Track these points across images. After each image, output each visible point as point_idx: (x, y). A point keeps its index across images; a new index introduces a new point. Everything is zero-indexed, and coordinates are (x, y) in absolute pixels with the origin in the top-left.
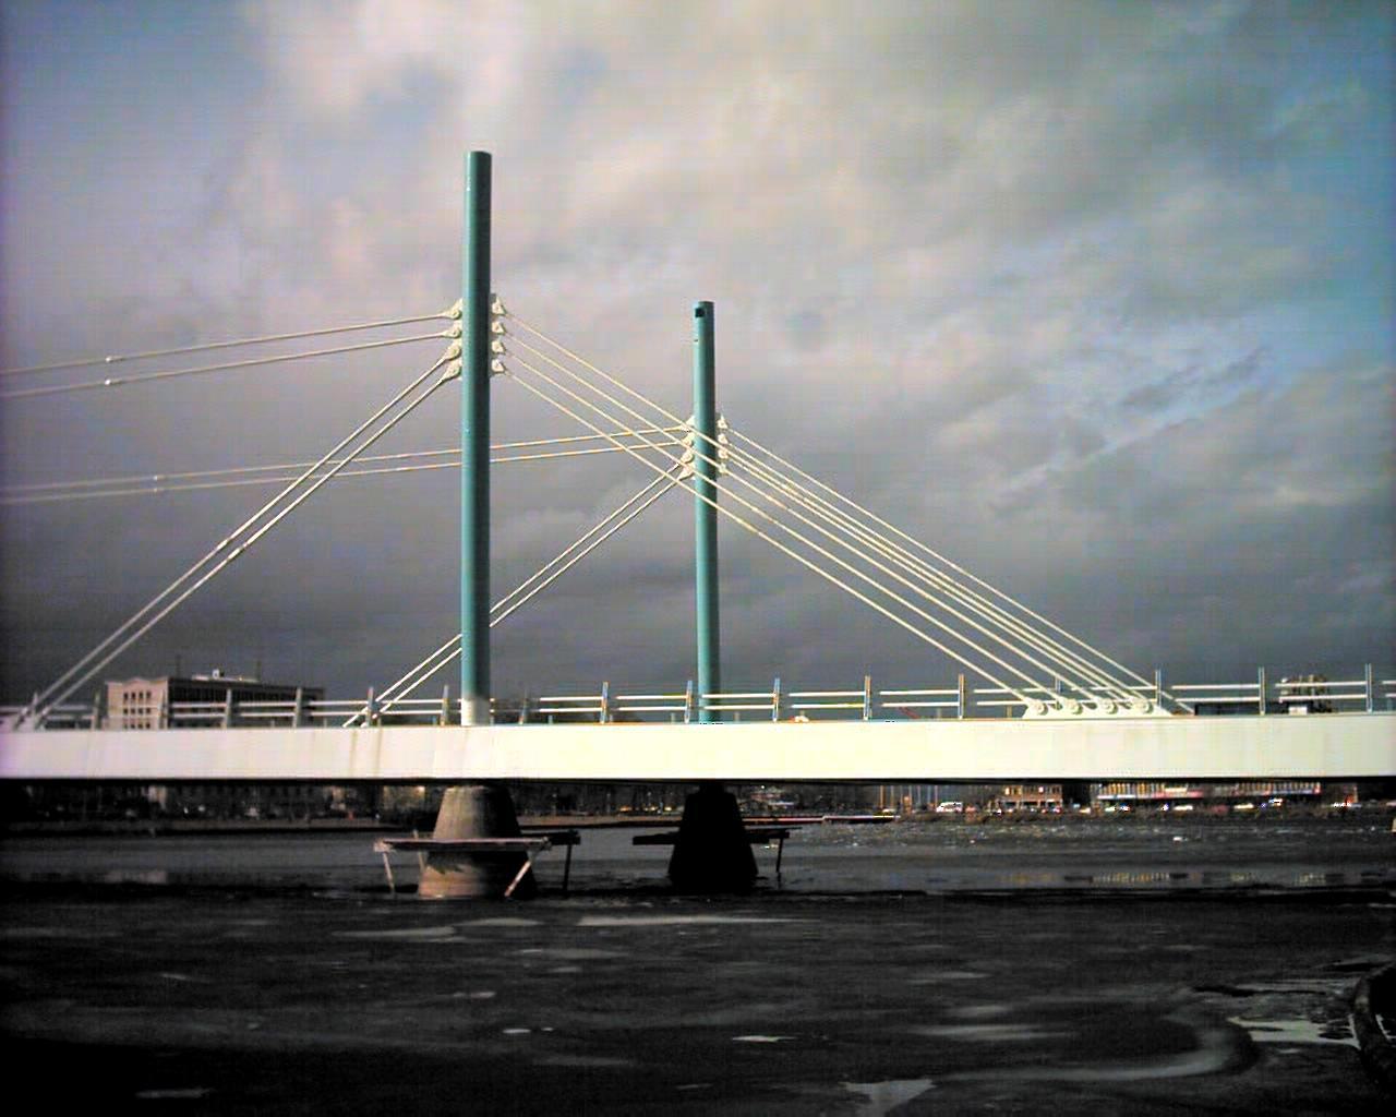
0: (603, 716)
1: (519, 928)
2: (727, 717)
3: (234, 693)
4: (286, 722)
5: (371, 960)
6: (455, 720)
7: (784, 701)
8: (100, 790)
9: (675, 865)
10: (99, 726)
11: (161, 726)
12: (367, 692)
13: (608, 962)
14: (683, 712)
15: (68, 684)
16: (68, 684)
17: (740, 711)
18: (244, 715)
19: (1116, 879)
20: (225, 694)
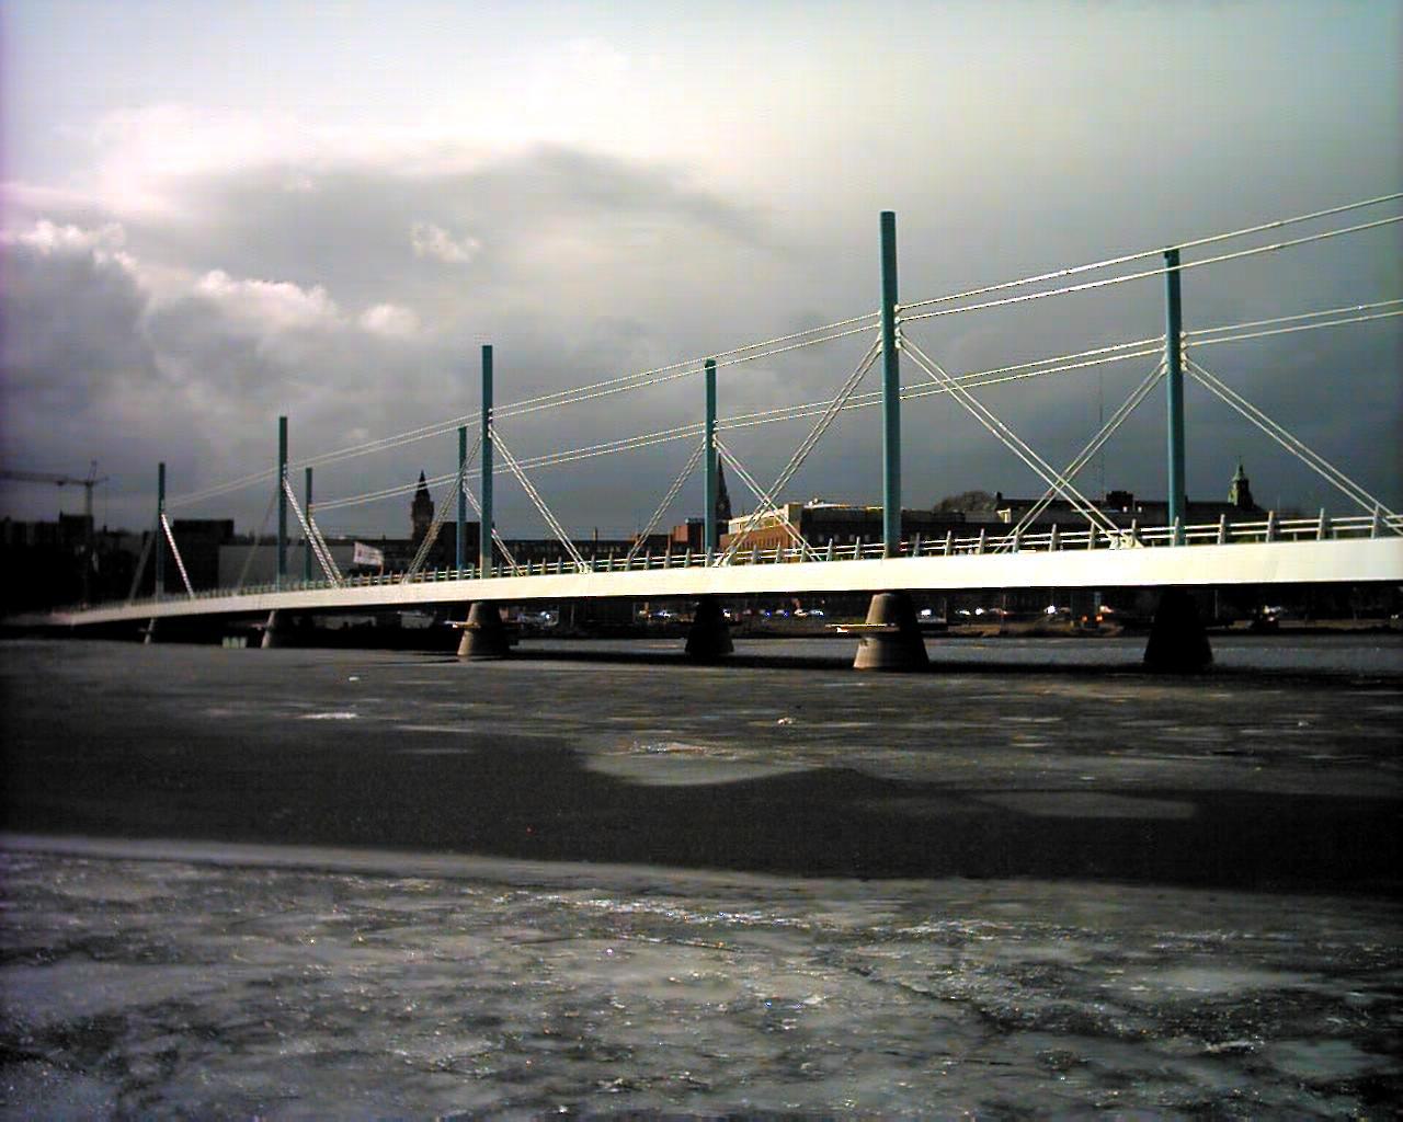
0: (1090, 545)
1: (856, 729)
2: (1288, 537)
3: (1275, 514)
4: (1213, 540)
5: (1070, 729)
6: (477, 577)
7: (1328, 524)
8: (1355, 589)
9: (1147, 656)
10: (709, 565)
11: (1222, 542)
12: (1319, 514)
13: (1131, 720)
14: (1265, 535)
15: (1038, 508)
16: (1038, 508)
17: (1298, 533)
18: (1283, 531)
19: (960, 682)
20: (1268, 514)
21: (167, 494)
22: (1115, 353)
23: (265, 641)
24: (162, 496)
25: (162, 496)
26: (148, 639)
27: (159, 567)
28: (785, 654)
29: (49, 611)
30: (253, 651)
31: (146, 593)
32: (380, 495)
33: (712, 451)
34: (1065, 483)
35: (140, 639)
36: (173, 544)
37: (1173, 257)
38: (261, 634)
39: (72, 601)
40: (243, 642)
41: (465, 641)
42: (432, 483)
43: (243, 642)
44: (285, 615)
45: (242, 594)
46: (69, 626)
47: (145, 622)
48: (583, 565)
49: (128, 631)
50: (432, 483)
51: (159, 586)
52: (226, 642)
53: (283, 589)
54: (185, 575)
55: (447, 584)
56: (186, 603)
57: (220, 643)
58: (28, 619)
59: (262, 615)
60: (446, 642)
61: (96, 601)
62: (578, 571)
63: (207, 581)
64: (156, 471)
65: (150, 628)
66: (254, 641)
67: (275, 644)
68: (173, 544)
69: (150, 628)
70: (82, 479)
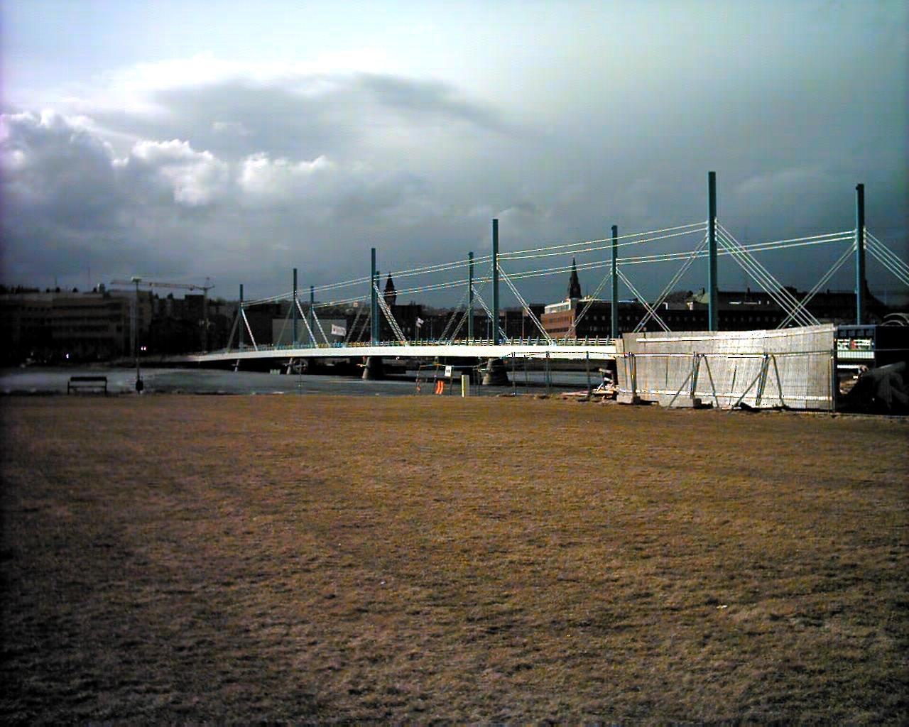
21: (298, 287)
22: (456, 283)
23: (288, 372)
24: (295, 289)
25: (295, 289)
26: (236, 369)
27: (241, 334)
28: (311, 376)
29: (188, 354)
30: (283, 376)
31: (235, 347)
32: (551, 271)
33: (615, 276)
34: (802, 307)
35: (232, 369)
36: (247, 324)
37: (471, 255)
38: (287, 368)
39: (197, 350)
40: (279, 371)
41: (236, 369)
42: (580, 267)
43: (279, 371)
44: (376, 360)
45: (278, 349)
46: (197, 362)
47: (234, 361)
48: (405, 342)
49: (227, 365)
50: (580, 267)
51: (241, 345)
52: (271, 371)
53: (296, 348)
54: (612, 317)
55: (393, 348)
56: (253, 353)
57: (269, 372)
58: (177, 358)
59: (287, 359)
60: (357, 373)
61: (210, 350)
62: (548, 344)
63: (266, 339)
64: (292, 272)
65: (237, 364)
66: (283, 372)
67: (370, 377)
68: (247, 324)
69: (237, 364)
70: (202, 286)
